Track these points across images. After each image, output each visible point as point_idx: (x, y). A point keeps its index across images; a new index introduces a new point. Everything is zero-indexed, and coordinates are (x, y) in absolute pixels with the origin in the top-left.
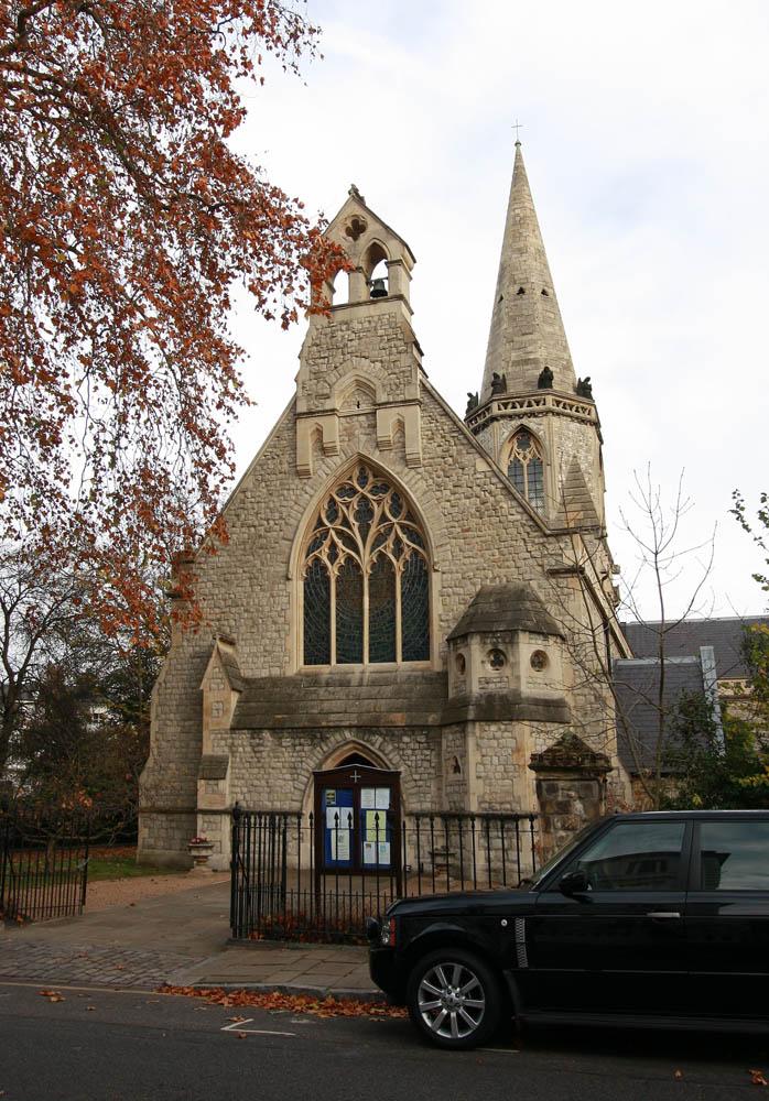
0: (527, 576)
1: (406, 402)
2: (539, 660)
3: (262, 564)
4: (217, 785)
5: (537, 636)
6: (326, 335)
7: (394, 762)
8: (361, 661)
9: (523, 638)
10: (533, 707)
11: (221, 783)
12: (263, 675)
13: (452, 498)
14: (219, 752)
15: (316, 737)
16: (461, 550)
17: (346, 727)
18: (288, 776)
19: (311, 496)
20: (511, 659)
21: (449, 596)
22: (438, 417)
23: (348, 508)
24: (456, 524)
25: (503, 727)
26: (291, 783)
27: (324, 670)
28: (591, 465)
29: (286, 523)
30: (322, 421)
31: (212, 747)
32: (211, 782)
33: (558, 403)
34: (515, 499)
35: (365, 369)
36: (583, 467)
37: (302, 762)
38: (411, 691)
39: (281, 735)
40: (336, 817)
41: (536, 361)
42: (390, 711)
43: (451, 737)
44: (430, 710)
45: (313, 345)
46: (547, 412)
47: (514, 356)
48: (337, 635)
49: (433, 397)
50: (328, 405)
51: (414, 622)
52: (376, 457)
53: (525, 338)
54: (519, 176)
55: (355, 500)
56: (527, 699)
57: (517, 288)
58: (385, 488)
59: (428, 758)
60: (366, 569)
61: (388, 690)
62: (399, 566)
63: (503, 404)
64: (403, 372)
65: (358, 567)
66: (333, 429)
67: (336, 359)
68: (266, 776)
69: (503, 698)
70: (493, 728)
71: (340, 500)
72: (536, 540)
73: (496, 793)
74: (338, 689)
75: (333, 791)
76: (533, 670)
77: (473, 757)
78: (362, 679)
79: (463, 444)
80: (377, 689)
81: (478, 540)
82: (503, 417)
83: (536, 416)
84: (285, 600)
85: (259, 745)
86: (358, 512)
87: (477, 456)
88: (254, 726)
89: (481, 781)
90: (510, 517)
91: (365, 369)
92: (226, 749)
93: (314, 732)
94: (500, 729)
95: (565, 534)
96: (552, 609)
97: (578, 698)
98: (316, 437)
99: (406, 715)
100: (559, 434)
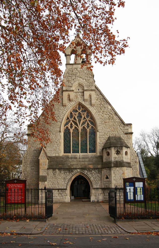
0: (120, 134)
1: (92, 90)
2: (126, 153)
3: (53, 128)
4: (44, 183)
6: (70, 71)
8: (79, 153)
9: (124, 148)
10: (126, 164)
11: (46, 182)
12: (54, 156)
13: (102, 114)
14: (44, 175)
15: (70, 171)
16: (104, 127)
17: (78, 168)
18: (63, 180)
19: (66, 112)
20: (121, 153)
21: (101, 138)
22: (99, 95)
23: (75, 115)
24: (103, 121)
25: (120, 168)
26: (64, 182)
29: (60, 118)
30: (70, 93)
31: (42, 173)
32: (43, 182)
35: (81, 81)
38: (93, 160)
39: (61, 170)
40: (130, 189)
42: (89, 165)
43: (105, 171)
44: (98, 164)
45: (67, 73)
48: (72, 146)
49: (98, 89)
50: (71, 89)
51: (92, 144)
52: (83, 103)
55: (77, 113)
56: (125, 162)
58: (85, 111)
60: (80, 130)
61: (87, 160)
62: (88, 130)
64: (91, 82)
65: (78, 130)
66: (72, 95)
67: (73, 77)
68: (57, 180)
69: (119, 162)
70: (118, 168)
71: (73, 113)
72: (122, 126)
73: (118, 183)
74: (74, 159)
75: (128, 183)
77: (113, 175)
78: (80, 157)
79: (105, 102)
80: (84, 159)
81: (108, 125)
84: (59, 137)
85: (55, 173)
86: (78, 116)
87: (108, 105)
88: (53, 168)
90: (116, 120)
91: (81, 81)
92: (46, 174)
93: (70, 170)
95: (129, 125)
98: (68, 96)
99: (93, 166)
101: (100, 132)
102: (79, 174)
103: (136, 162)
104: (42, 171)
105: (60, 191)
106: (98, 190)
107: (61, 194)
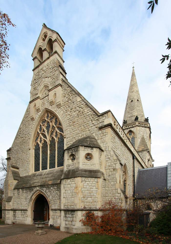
2: (89, 157)
3: (24, 147)
5: (88, 148)
7: (49, 195)
11: (10, 203)
12: (25, 176)
17: (37, 186)
18: (25, 200)
20: (77, 156)
25: (72, 180)
27: (38, 172)
28: (147, 137)
32: (8, 203)
33: (139, 124)
34: (89, 107)
36: (145, 137)
37: (28, 196)
41: (134, 116)
42: (49, 181)
46: (136, 126)
47: (129, 116)
52: (50, 108)
53: (132, 111)
54: (133, 75)
57: (131, 101)
59: (57, 193)
60: (49, 143)
63: (126, 126)
70: (69, 181)
76: (85, 160)
81: (77, 125)
82: (125, 129)
83: (133, 127)
89: (65, 199)
92: (13, 194)
93: (30, 188)
94: (71, 181)
96: (99, 141)
97: (107, 170)
100: (139, 131)
101: (67, 138)
102: (38, 192)
103: (114, 169)
104: (10, 191)
105: (22, 211)
106: (56, 211)
107: (23, 215)
